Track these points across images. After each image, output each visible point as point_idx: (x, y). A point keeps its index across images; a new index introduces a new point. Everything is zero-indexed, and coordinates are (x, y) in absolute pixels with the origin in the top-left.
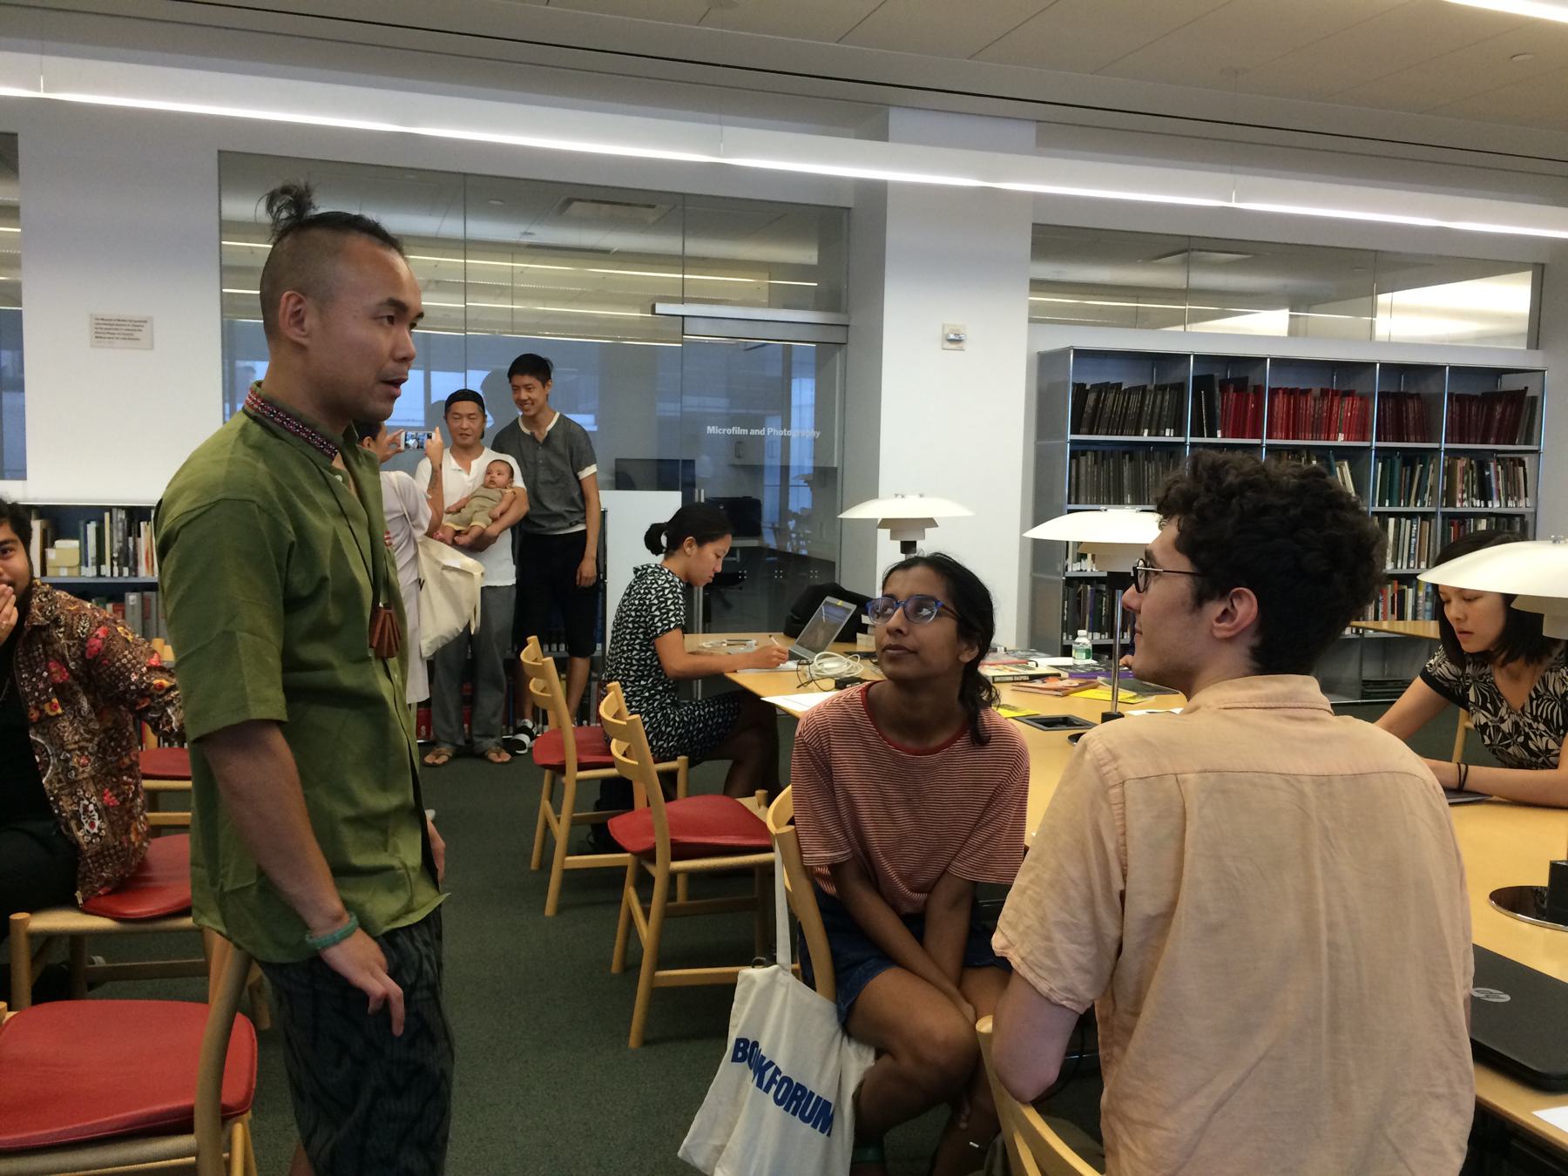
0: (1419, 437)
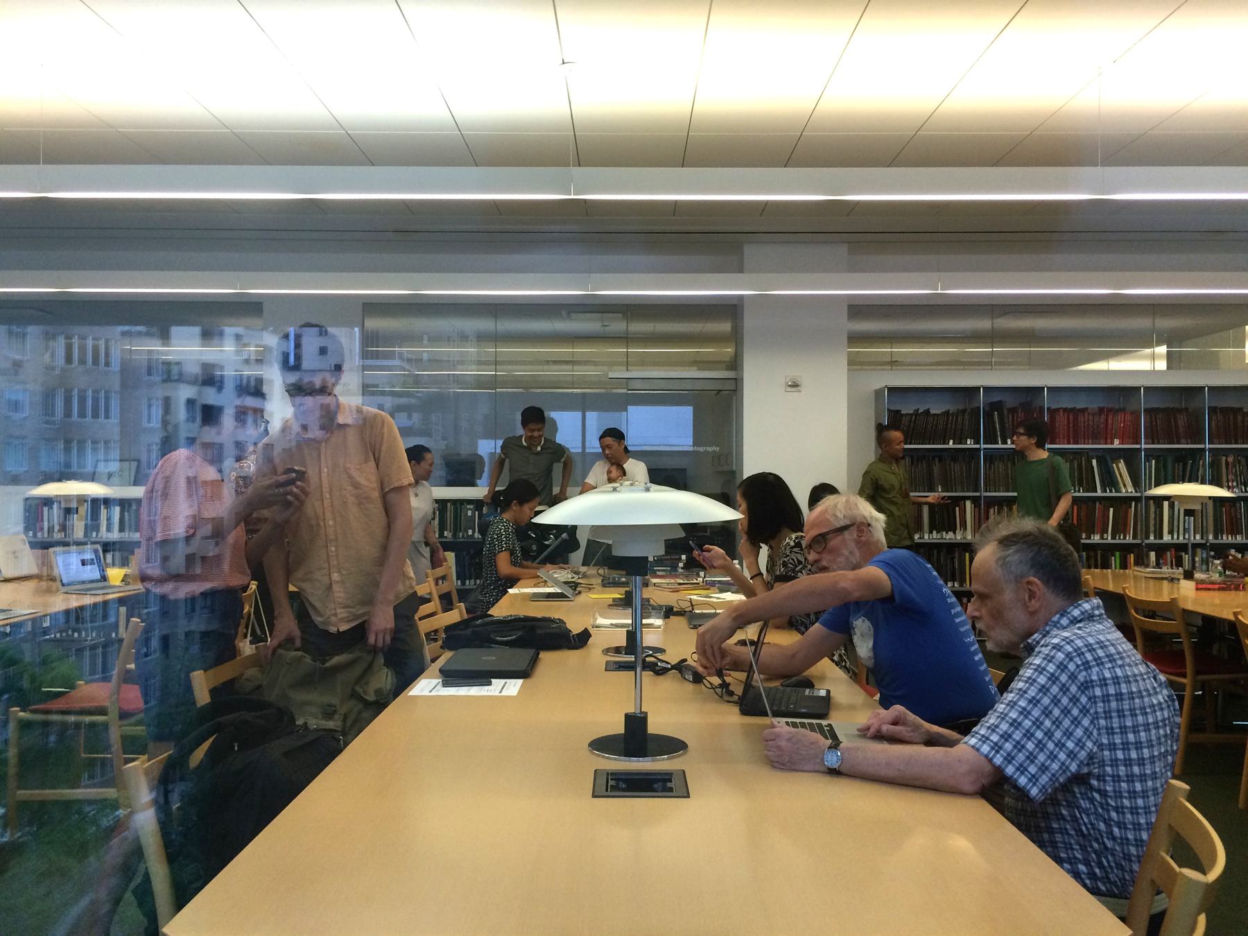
0: (1189, 441)
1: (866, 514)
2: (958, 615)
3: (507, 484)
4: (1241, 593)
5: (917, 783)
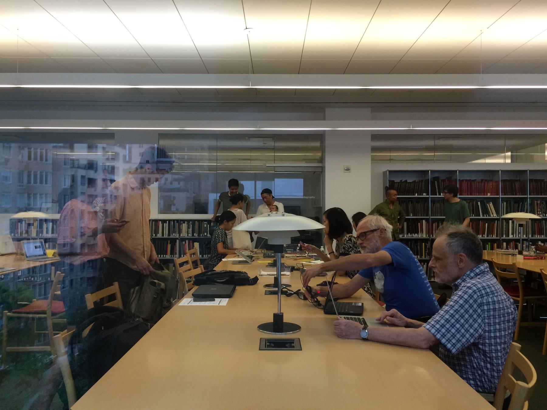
1: (385, 225)
2: (421, 271)
3: (222, 212)
4: (544, 261)
5: (402, 344)
